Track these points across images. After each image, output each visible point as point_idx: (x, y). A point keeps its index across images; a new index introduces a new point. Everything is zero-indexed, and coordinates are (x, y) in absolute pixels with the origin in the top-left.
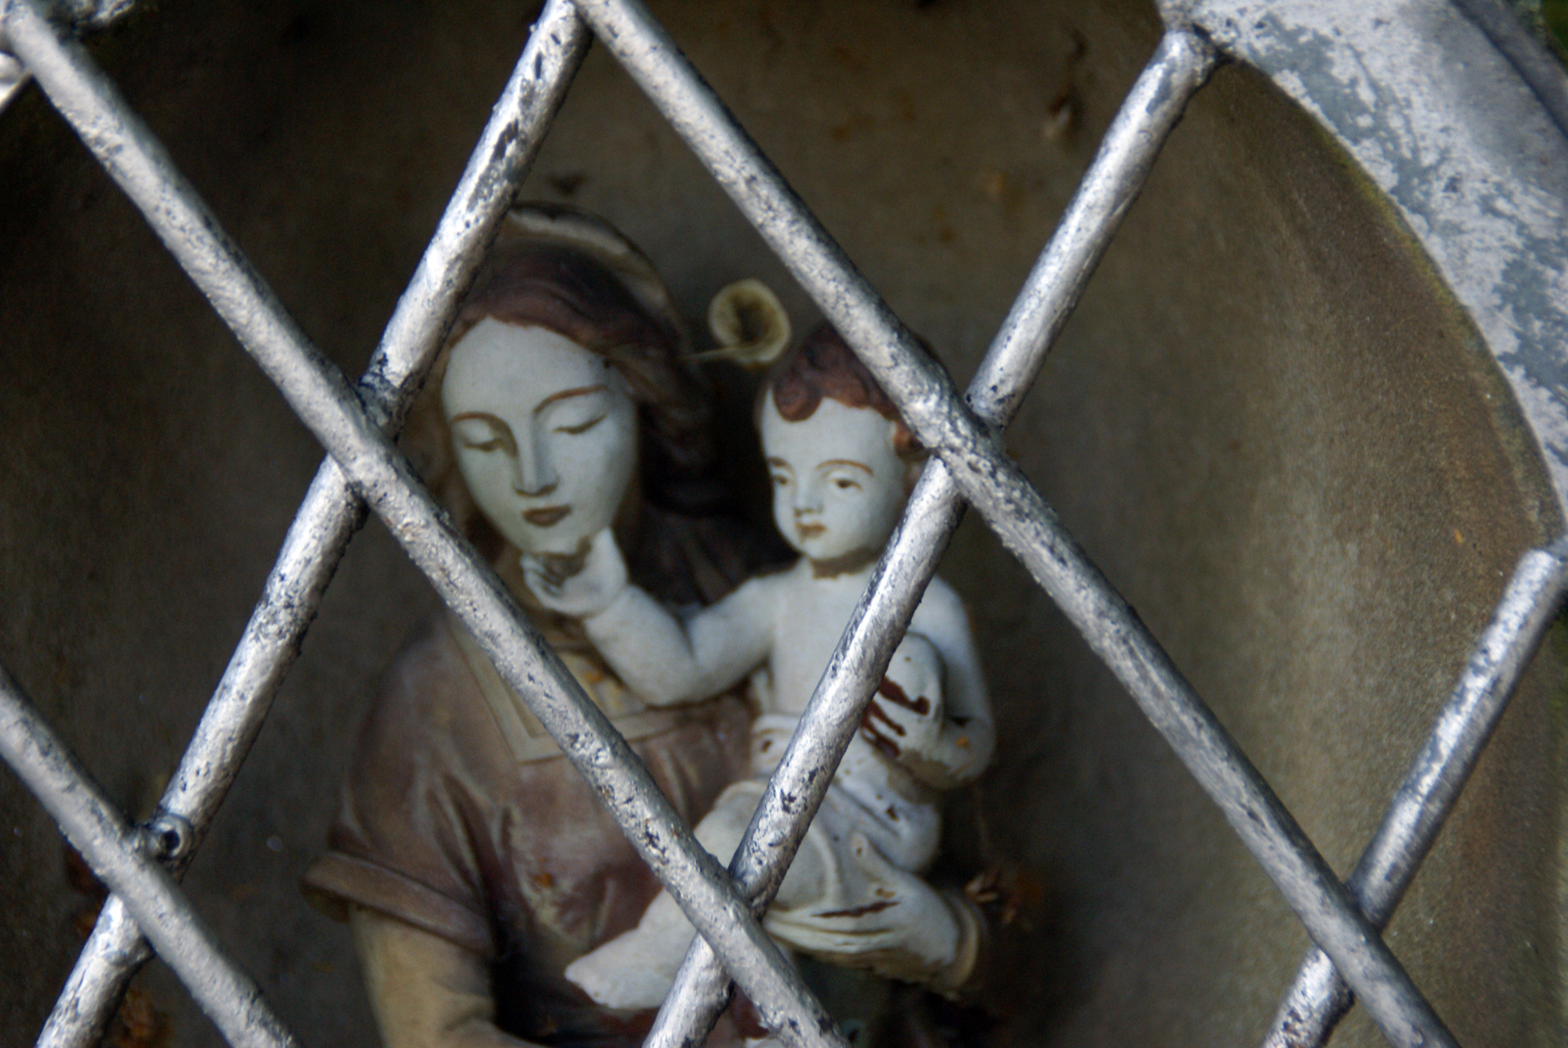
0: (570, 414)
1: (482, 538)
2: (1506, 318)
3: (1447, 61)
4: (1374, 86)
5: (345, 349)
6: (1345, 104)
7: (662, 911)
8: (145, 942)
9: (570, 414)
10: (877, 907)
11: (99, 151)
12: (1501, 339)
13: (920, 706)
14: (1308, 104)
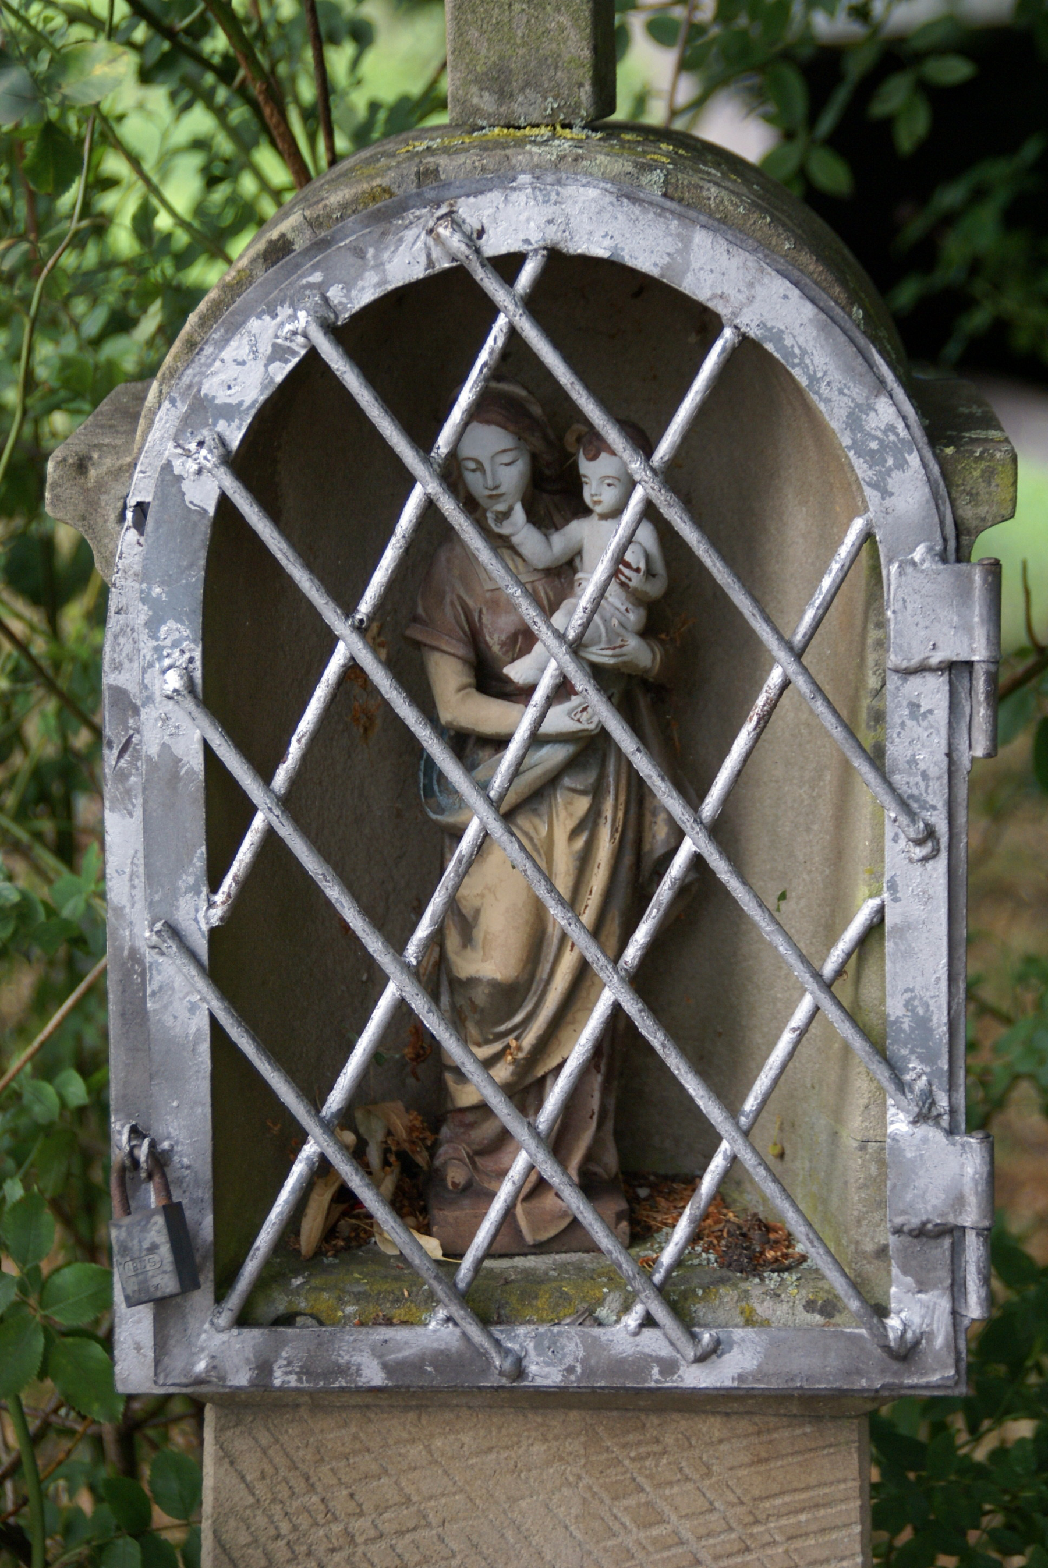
0: (506, 458)
1: (471, 505)
2: (848, 432)
3: (826, 339)
4: (800, 347)
5: (424, 441)
6: (789, 354)
7: (538, 647)
8: (352, 658)
9: (506, 458)
10: (621, 646)
11: (338, 373)
12: (846, 441)
13: (638, 570)
14: (777, 355)
